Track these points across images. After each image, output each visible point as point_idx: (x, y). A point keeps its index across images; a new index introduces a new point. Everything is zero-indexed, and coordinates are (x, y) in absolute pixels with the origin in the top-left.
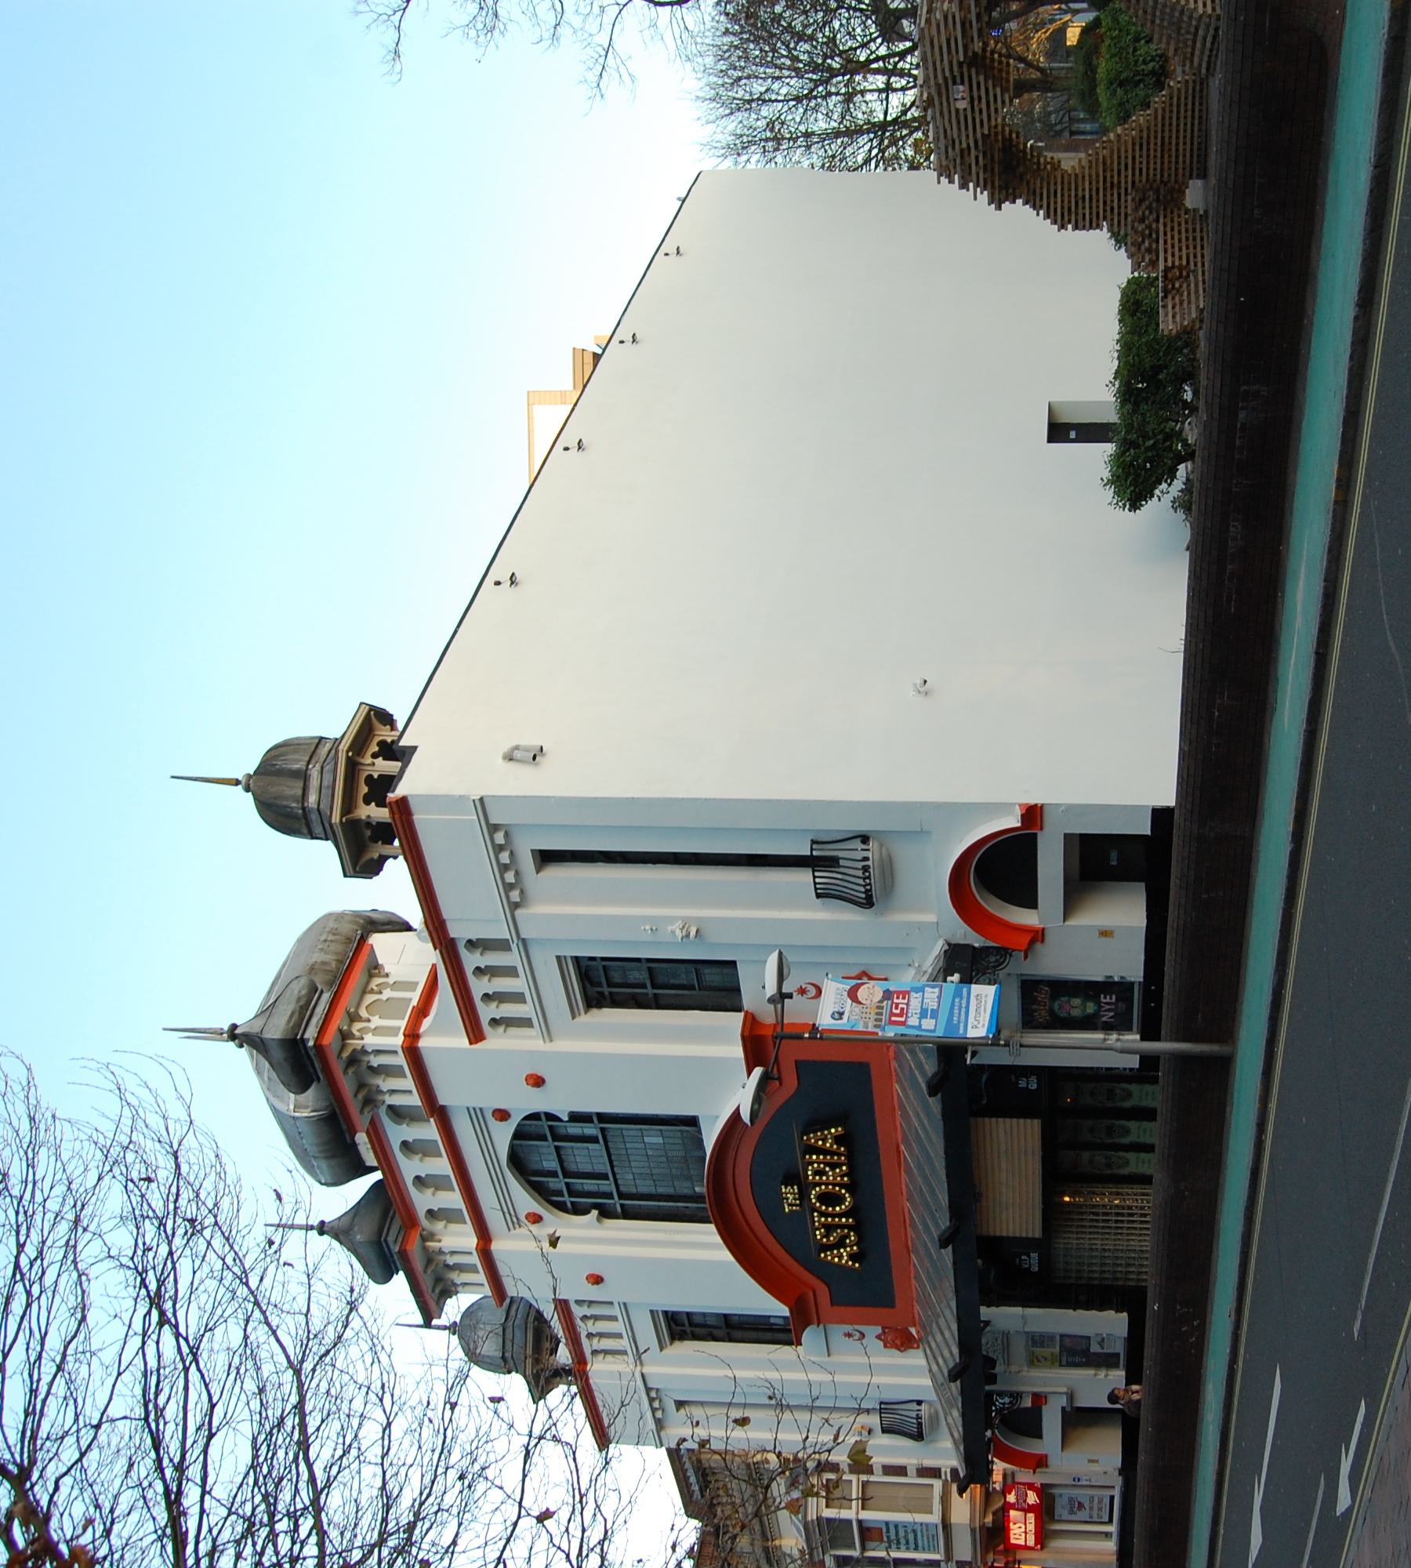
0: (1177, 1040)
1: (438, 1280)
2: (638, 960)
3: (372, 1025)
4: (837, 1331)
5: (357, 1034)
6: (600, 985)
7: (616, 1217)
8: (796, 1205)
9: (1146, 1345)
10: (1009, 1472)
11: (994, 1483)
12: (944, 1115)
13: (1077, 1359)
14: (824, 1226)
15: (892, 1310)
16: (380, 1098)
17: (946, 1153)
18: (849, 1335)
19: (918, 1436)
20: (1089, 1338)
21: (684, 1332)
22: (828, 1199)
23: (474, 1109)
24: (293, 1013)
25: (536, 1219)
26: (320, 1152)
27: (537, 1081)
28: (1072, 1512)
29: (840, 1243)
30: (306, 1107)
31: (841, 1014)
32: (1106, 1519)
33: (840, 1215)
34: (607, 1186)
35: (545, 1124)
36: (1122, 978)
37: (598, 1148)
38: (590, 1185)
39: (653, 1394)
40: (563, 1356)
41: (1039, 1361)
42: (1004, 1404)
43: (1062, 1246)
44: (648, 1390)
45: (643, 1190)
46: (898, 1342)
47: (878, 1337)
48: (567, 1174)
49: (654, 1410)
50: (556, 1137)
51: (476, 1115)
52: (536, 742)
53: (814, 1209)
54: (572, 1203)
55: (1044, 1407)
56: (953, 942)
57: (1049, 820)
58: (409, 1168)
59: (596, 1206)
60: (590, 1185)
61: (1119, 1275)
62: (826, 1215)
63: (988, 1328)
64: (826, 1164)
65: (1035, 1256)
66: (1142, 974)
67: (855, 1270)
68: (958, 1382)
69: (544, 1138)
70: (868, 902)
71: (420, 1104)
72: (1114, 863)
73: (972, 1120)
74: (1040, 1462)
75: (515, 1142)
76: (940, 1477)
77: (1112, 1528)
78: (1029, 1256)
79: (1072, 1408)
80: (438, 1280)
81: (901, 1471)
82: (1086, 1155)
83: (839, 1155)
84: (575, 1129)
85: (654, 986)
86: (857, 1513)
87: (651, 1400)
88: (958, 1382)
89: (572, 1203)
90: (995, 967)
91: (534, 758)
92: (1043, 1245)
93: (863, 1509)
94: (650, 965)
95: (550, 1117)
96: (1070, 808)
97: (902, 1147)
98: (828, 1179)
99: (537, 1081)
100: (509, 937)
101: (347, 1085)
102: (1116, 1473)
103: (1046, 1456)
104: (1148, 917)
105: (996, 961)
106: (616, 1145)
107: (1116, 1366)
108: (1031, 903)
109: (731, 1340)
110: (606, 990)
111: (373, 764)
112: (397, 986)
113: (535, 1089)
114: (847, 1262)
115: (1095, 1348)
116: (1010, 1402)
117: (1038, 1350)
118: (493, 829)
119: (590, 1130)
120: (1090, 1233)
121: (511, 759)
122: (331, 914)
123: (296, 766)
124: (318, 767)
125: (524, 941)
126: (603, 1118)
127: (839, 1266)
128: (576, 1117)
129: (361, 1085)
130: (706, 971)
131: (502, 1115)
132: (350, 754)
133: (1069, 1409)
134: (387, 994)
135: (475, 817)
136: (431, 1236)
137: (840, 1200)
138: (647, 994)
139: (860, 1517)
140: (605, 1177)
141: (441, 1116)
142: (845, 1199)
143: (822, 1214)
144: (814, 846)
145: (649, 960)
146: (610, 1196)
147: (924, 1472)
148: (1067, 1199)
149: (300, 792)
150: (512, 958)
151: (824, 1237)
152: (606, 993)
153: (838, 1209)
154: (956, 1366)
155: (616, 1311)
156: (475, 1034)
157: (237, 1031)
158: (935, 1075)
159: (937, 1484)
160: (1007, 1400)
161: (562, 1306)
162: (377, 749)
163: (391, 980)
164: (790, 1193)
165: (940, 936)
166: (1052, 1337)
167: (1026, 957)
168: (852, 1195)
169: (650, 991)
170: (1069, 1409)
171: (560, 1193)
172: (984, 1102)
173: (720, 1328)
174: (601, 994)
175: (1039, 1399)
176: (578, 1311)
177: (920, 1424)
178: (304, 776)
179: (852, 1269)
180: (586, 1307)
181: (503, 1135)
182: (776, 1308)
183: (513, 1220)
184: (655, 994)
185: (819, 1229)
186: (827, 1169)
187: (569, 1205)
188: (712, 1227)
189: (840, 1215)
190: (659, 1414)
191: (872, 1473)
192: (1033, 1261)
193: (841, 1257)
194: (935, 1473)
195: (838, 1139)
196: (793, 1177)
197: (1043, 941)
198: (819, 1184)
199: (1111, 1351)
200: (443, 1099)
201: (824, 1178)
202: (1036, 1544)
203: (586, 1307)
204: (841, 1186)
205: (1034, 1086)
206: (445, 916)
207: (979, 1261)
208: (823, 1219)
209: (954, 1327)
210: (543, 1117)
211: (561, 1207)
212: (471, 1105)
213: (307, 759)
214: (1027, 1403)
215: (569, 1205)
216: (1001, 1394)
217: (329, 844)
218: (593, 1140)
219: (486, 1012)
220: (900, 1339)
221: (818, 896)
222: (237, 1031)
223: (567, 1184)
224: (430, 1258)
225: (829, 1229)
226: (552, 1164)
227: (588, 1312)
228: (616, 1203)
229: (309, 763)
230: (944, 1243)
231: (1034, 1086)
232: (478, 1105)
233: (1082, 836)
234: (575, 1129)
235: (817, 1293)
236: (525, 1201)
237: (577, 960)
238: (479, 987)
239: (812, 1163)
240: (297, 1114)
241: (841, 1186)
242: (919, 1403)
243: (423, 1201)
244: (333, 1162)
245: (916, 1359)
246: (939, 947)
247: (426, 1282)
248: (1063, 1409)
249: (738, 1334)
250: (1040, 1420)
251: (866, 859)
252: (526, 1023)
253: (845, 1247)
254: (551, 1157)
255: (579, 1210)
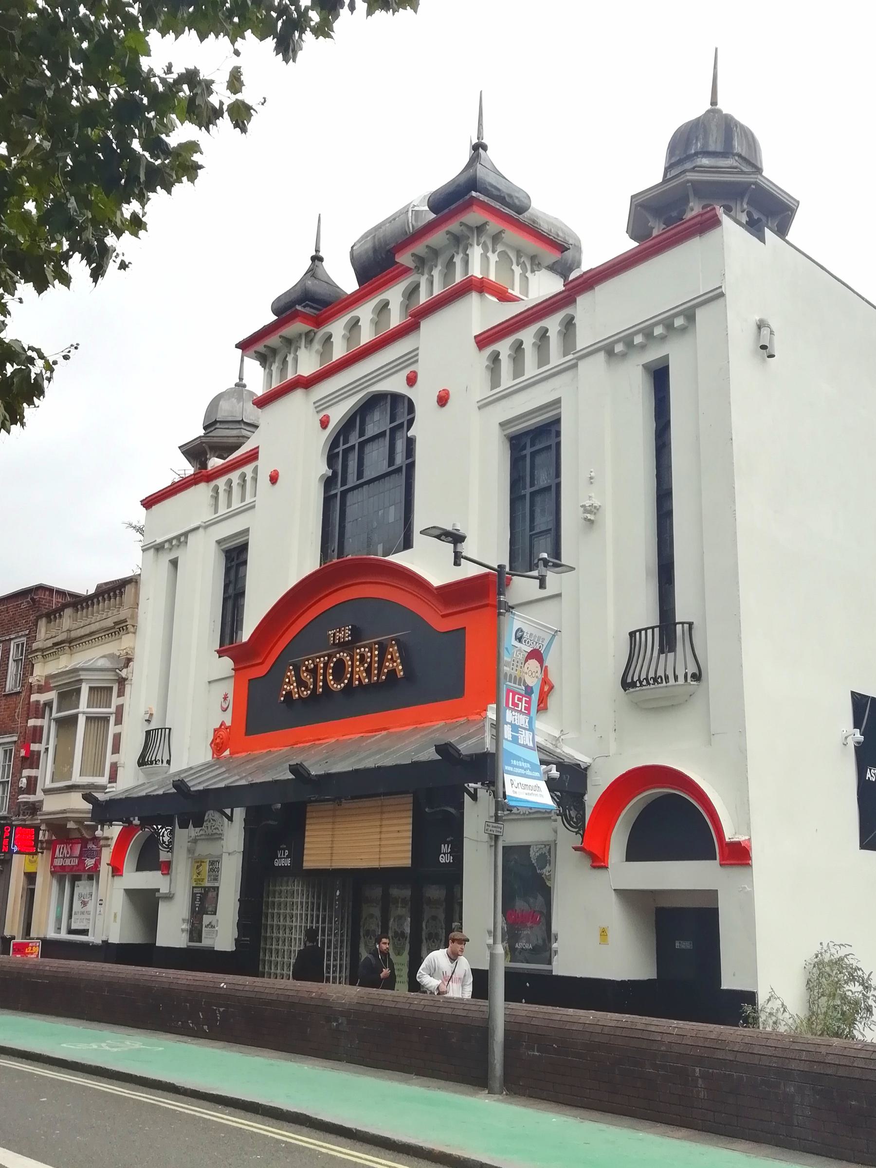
0: (506, 1023)
1: (274, 351)
2: (558, 474)
3: (490, 254)
4: (228, 688)
5: (482, 240)
6: (532, 445)
7: (326, 491)
8: (334, 640)
9: (189, 973)
10: (109, 842)
11: (102, 830)
12: (415, 765)
13: (198, 903)
14: (316, 667)
15: (244, 735)
16: (426, 270)
17: (379, 768)
18: (225, 698)
19: (142, 762)
20: (215, 914)
21: (233, 560)
22: (339, 670)
23: (417, 355)
24: (498, 190)
25: (324, 424)
26: (379, 239)
27: (443, 400)
28: (80, 896)
29: (301, 683)
30: (416, 220)
31: (519, 639)
32: (74, 927)
33: (325, 681)
34: (352, 481)
35: (403, 418)
36: (556, 952)
37: (384, 468)
38: (353, 465)
39: (182, 539)
40: (215, 462)
41: (198, 867)
42: (163, 836)
43: (295, 888)
44: (186, 534)
45: (349, 511)
46: (218, 741)
47: (223, 724)
48: (362, 445)
49: (170, 541)
50: (393, 431)
51: (412, 357)
52: (777, 350)
53: (330, 656)
54: (338, 452)
55: (160, 872)
56: (588, 773)
57: (735, 873)
58: (365, 312)
59: (335, 473)
60: (353, 465)
61: (268, 942)
62: (325, 668)
63: (226, 820)
64: (370, 664)
65: (287, 862)
66: (560, 974)
67: (279, 698)
68: (174, 790)
69: (392, 420)
70: (626, 684)
71: (421, 304)
72: (677, 944)
73: (409, 799)
74: (117, 871)
75: (389, 397)
76: (110, 782)
77: (64, 936)
78: (288, 857)
79: (159, 898)
80: (274, 351)
81: (116, 749)
82: (377, 912)
83: (379, 675)
84: (400, 446)
85: (533, 494)
86: (84, 713)
87: (178, 538)
88: (174, 790)
89: (338, 452)
90: (565, 815)
91: (764, 347)
92: (297, 870)
93: (87, 718)
94: (553, 489)
95: (411, 422)
96: (749, 898)
97: (384, 733)
98: (358, 666)
99: (443, 400)
100: (578, 349)
101: (438, 238)
102: (105, 939)
103: (121, 875)
104: (623, 982)
105: (572, 818)
106: (388, 483)
107: (191, 939)
108: (634, 854)
109: (225, 600)
110: (528, 451)
111: (743, 212)
112: (525, 279)
113: (436, 399)
114: (285, 690)
115: (207, 919)
116: (164, 842)
117: (206, 867)
118: (689, 315)
119: (400, 459)
120: (307, 915)
121: (759, 327)
122: (580, 241)
123: (736, 143)
124: (735, 164)
125: (575, 366)
126: (411, 467)
127: (282, 682)
128: (411, 443)
129: (435, 253)
130: (549, 539)
131: (412, 380)
132: (753, 187)
133: (157, 895)
134: (518, 270)
135: (701, 293)
136: (310, 341)
137: (338, 678)
138: (525, 488)
139: (80, 716)
140: (360, 475)
141: (410, 327)
142: (138, 103)
143: (326, 665)
144: (686, 626)
145: (558, 486)
146: (344, 483)
147: (114, 768)
148: (338, 893)
149: (712, 148)
150: (556, 358)
151: (307, 668)
152: (524, 452)
153: (335, 686)
154: (188, 787)
155: (248, 500)
156: (484, 341)
157: (481, 150)
158: (458, 751)
159: (103, 780)
160: (166, 839)
161: (253, 456)
162: (756, 217)
163: (528, 274)
164: (345, 634)
165: (594, 760)
166: (216, 879)
167: (576, 849)
168: (343, 690)
169: (528, 491)
170: (157, 895)
171: (346, 441)
172: (427, 810)
173: (235, 589)
174: (524, 448)
175: (166, 868)
176: (248, 469)
177: (152, 763)
178: (726, 153)
179: (279, 694)
180: (252, 475)
181: (395, 384)
182: (246, 634)
183: (322, 405)
184: (525, 495)
185: (313, 662)
186: (366, 665)
187: (337, 450)
188: (317, 567)
189: (325, 681)
190: (167, 546)
191: (116, 724)
192: (283, 861)
193: (289, 683)
194: (113, 778)
195: (392, 672)
196: (357, 635)
197: (594, 867)
198: (352, 659)
199: (204, 935)
200: (427, 326)
201: (358, 663)
202: (55, 867)
203: (252, 475)
204: (351, 680)
205: (442, 860)
206: (598, 288)
207: (279, 806)
208: (322, 665)
209: (222, 785)
210: (410, 416)
211: (334, 444)
212: (420, 351)
213: (743, 154)
214: (164, 856)
215: (337, 450)
216: (172, 833)
217: (659, 179)
218: (391, 461)
219: (504, 347)
220: (219, 745)
221: (632, 634)
222: (481, 150)
223: (353, 447)
224: (290, 343)
225: (313, 672)
226: (371, 431)
227: (248, 478)
228: (338, 490)
229: (740, 156)
230: (296, 769)
231: (442, 860)
232: (420, 357)
233: (718, 909)
234: (400, 446)
235: (260, 666)
236: (338, 414)
237: (557, 421)
238: (528, 336)
239: (371, 651)
240: (410, 214)
241: (351, 680)
242: (169, 762)
243: (337, 328)
244: (371, 253)
245: (205, 755)
246: (582, 758)
247: (273, 341)
248: (158, 890)
249: (230, 603)
250: (151, 870)
251: (676, 678)
252: (495, 381)
253: (297, 687)
254: (376, 429)
255: (331, 459)
